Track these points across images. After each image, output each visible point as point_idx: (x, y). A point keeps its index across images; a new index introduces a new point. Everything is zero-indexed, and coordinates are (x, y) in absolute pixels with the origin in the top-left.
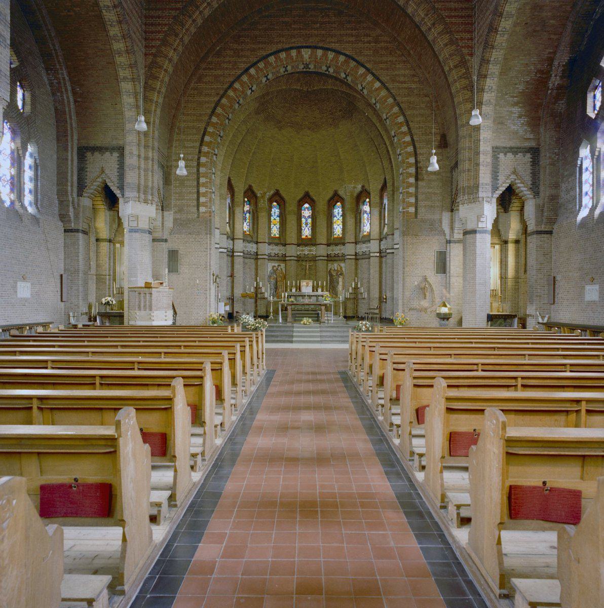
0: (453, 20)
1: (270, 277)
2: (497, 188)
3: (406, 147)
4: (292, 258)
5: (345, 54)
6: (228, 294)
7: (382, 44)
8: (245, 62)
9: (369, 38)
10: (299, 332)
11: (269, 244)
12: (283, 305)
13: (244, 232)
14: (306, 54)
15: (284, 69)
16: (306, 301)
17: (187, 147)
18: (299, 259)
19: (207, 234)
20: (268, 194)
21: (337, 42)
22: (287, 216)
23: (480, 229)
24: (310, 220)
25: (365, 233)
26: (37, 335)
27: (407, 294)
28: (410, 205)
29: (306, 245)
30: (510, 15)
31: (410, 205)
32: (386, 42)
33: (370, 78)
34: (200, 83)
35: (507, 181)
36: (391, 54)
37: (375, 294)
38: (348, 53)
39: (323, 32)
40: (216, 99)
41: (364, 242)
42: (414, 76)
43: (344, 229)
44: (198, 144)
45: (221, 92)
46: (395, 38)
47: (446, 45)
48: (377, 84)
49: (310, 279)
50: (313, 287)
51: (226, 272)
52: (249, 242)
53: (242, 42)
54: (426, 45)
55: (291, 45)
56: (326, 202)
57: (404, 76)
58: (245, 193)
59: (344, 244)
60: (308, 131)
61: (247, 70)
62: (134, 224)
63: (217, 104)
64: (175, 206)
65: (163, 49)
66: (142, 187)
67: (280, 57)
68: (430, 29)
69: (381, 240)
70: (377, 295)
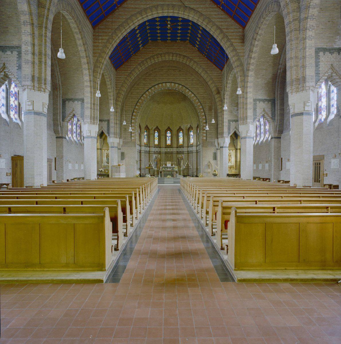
0: (216, 79)
1: (154, 160)
2: (230, 133)
3: (202, 117)
4: (164, 153)
6: (139, 167)
9: (190, 80)
10: (166, 180)
11: (154, 147)
12: (160, 171)
14: (168, 85)
16: (169, 170)
17: (127, 117)
18: (166, 153)
19: (134, 147)
20: (154, 128)
22: (161, 136)
23: (306, 112)
24: (170, 138)
25: (192, 143)
27: (203, 167)
28: (204, 136)
29: (168, 148)
31: (204, 136)
35: (261, 114)
38: (182, 84)
40: (137, 100)
41: (191, 147)
42: (205, 92)
43: (183, 141)
44: (131, 116)
49: (170, 161)
51: (139, 159)
55: (163, 82)
56: (176, 131)
58: (145, 128)
59: (183, 147)
62: (113, 145)
63: (138, 102)
65: (122, 88)
69: (197, 146)
70: (196, 167)
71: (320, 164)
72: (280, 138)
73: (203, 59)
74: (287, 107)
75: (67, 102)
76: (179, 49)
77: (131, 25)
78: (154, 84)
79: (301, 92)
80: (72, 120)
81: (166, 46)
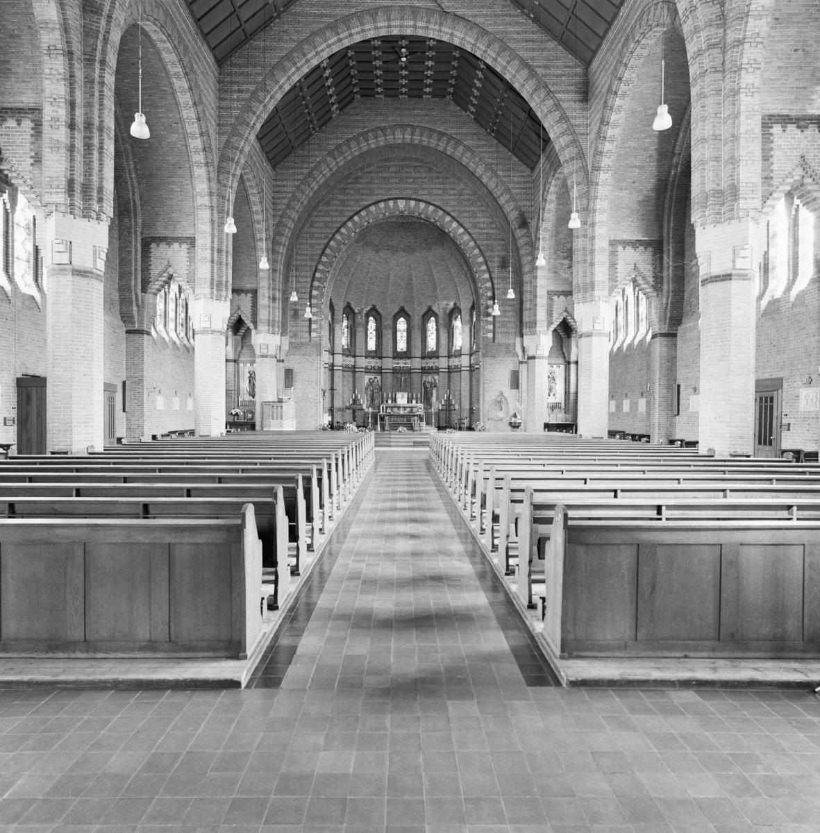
1: (367, 389)
3: (485, 283)
6: (328, 405)
11: (366, 357)
13: (343, 346)
14: (401, 204)
16: (402, 412)
18: (395, 371)
24: (405, 334)
26: (8, 460)
30: (551, 201)
32: (469, 194)
37: (466, 406)
38: (436, 203)
39: (416, 186)
40: (326, 241)
42: (492, 223)
44: (309, 280)
45: (330, 236)
49: (404, 391)
50: (408, 398)
52: (348, 356)
57: (484, 223)
59: (437, 357)
60: (404, 254)
62: (264, 352)
63: (327, 245)
64: (291, 331)
65: (288, 211)
66: (215, 283)
69: (471, 355)
70: (467, 407)
71: (772, 399)
72: (675, 335)
73: (485, 140)
74: (691, 261)
75: (153, 245)
76: (427, 115)
77: (312, 58)
78: (366, 203)
79: (727, 223)
80: (167, 290)
81: (397, 109)
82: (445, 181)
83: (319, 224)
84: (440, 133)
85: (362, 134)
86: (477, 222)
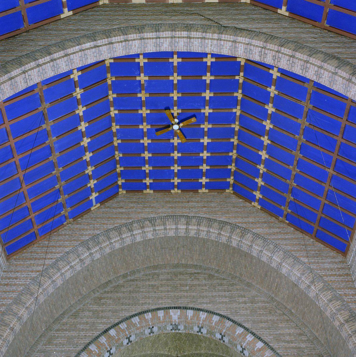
0: (332, 278)
5: (218, 314)
7: (260, 304)
8: (104, 323)
9: (244, 299)
14: (175, 315)
15: (149, 330)
21: (209, 303)
32: (264, 302)
33: (250, 338)
34: (49, 345)
36: (270, 313)
42: (300, 334)
46: (272, 298)
47: (330, 301)
48: (260, 345)
53: (103, 304)
54: (308, 303)
55: (157, 306)
57: (290, 334)
61: (106, 331)
65: (14, 307)
67: (145, 318)
68: (309, 287)
73: (279, 228)
76: (205, 207)
78: (128, 314)
81: (167, 202)
82: (230, 288)
83: (59, 340)
84: (221, 222)
85: (125, 225)
86: (280, 334)
